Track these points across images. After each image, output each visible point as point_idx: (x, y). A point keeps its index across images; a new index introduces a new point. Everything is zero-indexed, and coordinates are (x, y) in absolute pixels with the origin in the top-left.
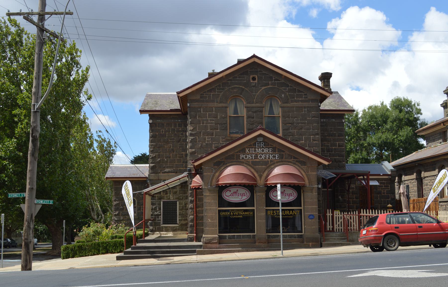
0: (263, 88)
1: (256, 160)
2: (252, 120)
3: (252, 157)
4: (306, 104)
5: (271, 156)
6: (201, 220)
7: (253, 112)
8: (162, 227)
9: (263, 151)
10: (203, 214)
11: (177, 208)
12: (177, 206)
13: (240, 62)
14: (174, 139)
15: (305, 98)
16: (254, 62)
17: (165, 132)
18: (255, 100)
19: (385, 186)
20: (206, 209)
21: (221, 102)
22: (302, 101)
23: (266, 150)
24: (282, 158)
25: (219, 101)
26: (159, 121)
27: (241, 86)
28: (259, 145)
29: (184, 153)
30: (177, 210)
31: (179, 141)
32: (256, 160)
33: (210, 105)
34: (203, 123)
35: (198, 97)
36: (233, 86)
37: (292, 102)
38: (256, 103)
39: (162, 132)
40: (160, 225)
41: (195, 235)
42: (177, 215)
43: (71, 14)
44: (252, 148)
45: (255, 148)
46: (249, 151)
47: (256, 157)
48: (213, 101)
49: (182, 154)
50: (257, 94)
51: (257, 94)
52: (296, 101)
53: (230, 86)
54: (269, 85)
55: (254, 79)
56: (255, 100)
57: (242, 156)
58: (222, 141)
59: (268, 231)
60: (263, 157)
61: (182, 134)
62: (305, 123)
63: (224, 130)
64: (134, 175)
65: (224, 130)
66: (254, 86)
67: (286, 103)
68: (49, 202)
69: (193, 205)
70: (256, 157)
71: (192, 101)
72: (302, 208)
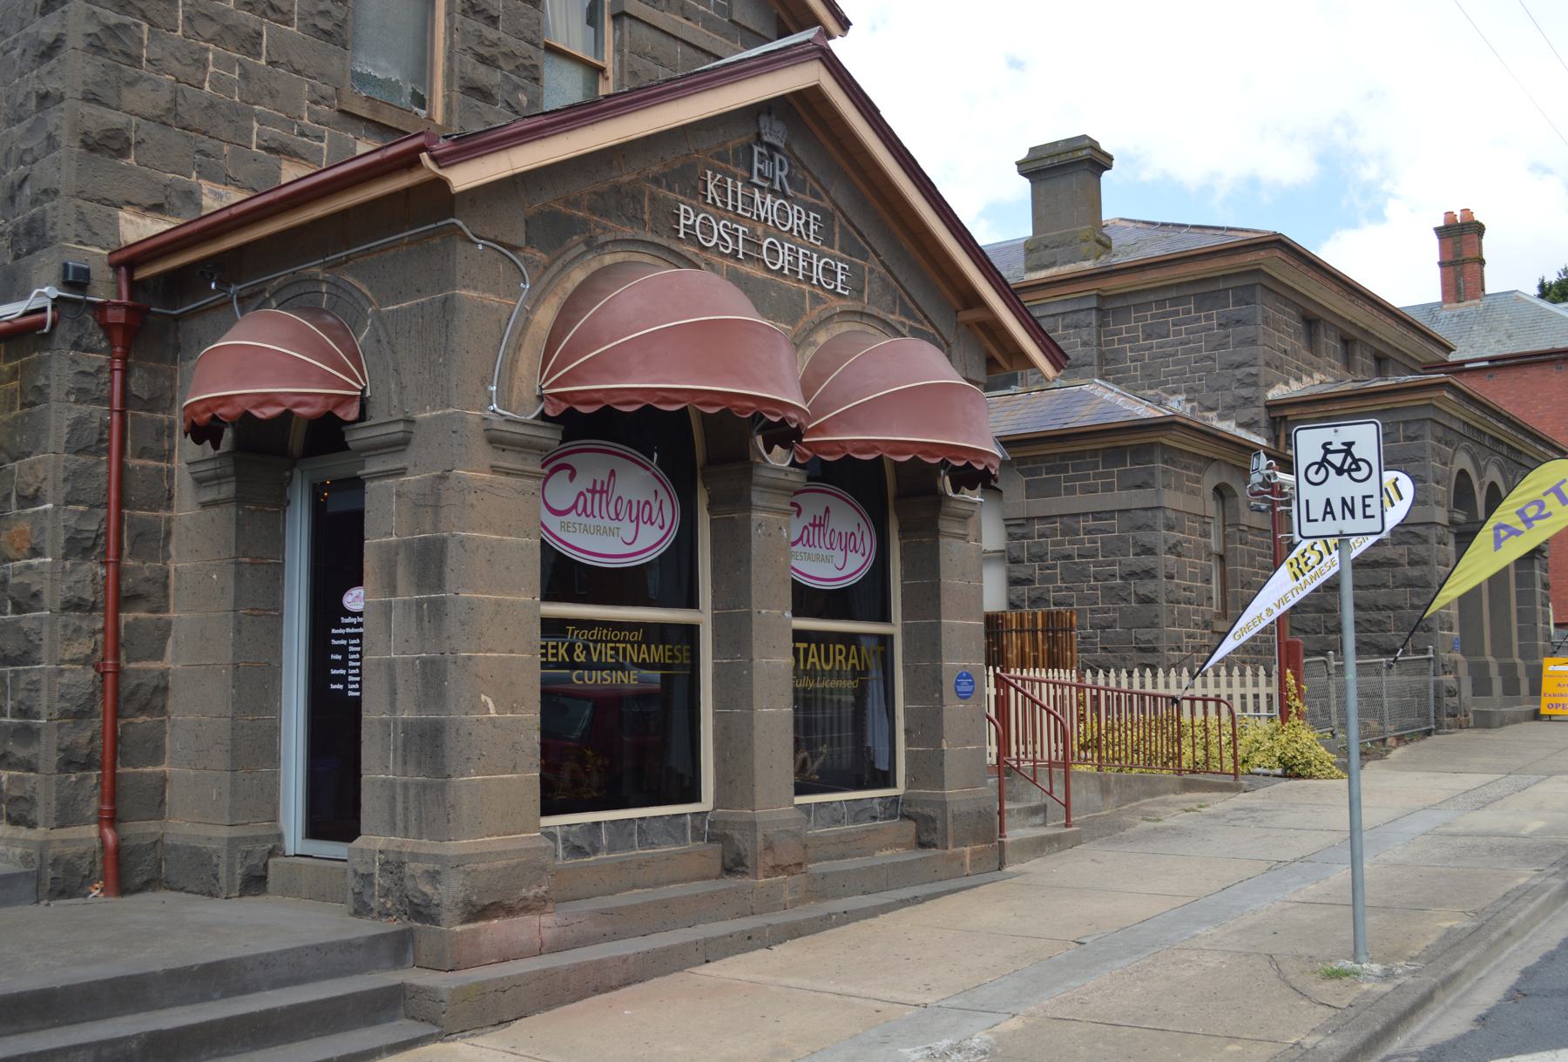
2: (490, 33)
5: (818, 265)
6: (143, 709)
10: (159, 654)
20: (471, 606)
46: (721, 188)
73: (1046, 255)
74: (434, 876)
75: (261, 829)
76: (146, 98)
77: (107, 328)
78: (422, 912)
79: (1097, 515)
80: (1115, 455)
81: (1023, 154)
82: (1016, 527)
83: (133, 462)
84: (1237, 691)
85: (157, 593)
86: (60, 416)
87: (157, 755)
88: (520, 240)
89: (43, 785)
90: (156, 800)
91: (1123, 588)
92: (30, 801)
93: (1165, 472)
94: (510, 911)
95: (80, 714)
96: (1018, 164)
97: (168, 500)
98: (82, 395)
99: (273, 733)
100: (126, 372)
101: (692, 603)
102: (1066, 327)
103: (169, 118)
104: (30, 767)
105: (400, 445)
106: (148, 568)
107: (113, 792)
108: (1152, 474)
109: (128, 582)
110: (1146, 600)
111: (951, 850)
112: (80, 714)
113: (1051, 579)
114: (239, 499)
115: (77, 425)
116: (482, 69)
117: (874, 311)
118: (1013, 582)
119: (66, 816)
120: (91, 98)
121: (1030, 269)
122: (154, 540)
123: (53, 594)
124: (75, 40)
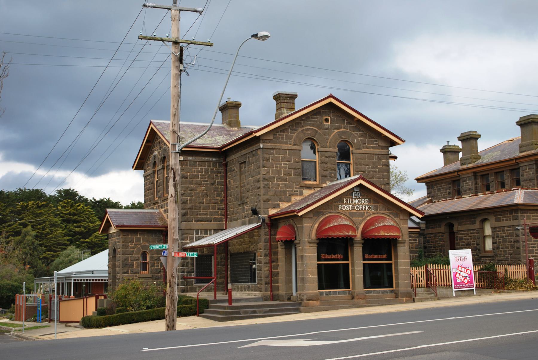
0: (336, 131)
1: (353, 211)
2: (326, 166)
3: (349, 207)
4: (377, 151)
5: (367, 208)
6: (276, 276)
7: (327, 157)
8: (196, 288)
9: (359, 201)
10: (277, 269)
11: (211, 264)
12: (211, 261)
14: (207, 181)
15: (375, 144)
16: (331, 104)
17: (198, 172)
18: (328, 145)
19: (413, 240)
20: (307, 263)
21: (295, 145)
22: (373, 148)
23: (362, 201)
24: (377, 209)
25: (292, 143)
26: (190, 158)
27: (314, 128)
28: (356, 195)
29: (219, 198)
30: (211, 266)
31: (213, 184)
32: (353, 211)
33: (284, 146)
34: (276, 167)
35: (271, 137)
36: (306, 127)
37: (364, 148)
38: (330, 147)
39: (195, 172)
40: (192, 285)
41: (269, 292)
42: (212, 272)
44: (349, 198)
45: (352, 198)
46: (347, 201)
47: (353, 207)
48: (286, 143)
49: (217, 200)
50: (331, 137)
51: (331, 137)
52: (367, 148)
53: (303, 127)
54: (341, 128)
55: (327, 120)
56: (328, 145)
57: (340, 206)
58: (296, 188)
60: (360, 208)
61: (217, 176)
62: (375, 172)
63: (297, 175)
65: (297, 175)
66: (326, 129)
67: (359, 148)
68: (193, 255)
69: (488, 252)
70: (353, 207)
71: (264, 142)
72: (392, 262)
73: (524, 149)
74: (303, 296)
75: (290, 292)
76: (271, 193)
77: (268, 226)
78: (302, 300)
79: (509, 227)
80: (511, 212)
81: (518, 120)
82: (494, 229)
83: (272, 243)
84: (420, 271)
85: (277, 260)
86: (263, 238)
87: (277, 282)
88: (312, 216)
89: (263, 286)
90: (278, 289)
91: (514, 245)
92: (261, 288)
93: (521, 216)
94: (313, 300)
95: (267, 277)
96: (517, 122)
97: (277, 248)
98: (265, 235)
99: (291, 279)
100: (271, 231)
101: (348, 260)
102: (529, 169)
103: (275, 194)
104: (261, 284)
105: (299, 243)
106: (275, 257)
107: (271, 287)
108: (518, 217)
109: (272, 260)
110: (518, 248)
111: (400, 298)
112: (267, 277)
113: (500, 242)
114: (285, 248)
115: (265, 239)
116: (325, 172)
117: (381, 212)
118: (493, 243)
119: (266, 290)
120: (264, 195)
121: (521, 152)
122: (276, 253)
123: (263, 262)
124: (262, 187)
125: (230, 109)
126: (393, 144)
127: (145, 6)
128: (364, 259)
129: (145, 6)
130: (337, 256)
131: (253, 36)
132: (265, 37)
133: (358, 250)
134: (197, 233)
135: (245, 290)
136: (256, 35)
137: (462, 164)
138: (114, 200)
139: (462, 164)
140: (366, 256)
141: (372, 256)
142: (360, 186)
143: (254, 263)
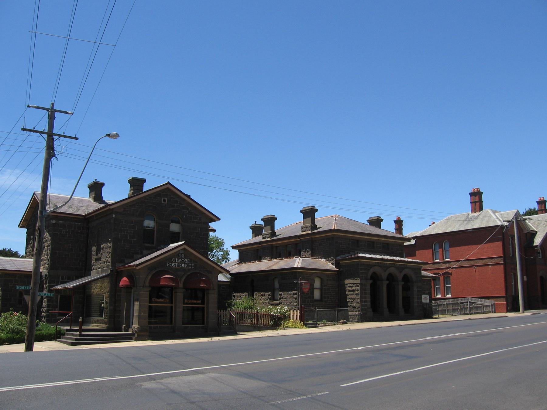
5: (188, 266)
9: (183, 261)
13: (189, 196)
16: (168, 188)
23: (185, 261)
43: (77, 139)
55: (164, 201)
59: (183, 324)
60: (183, 265)
64: (24, 268)
72: (205, 306)
73: (304, 229)
125: (96, 189)
126: (212, 221)
127: (29, 106)
128: (184, 303)
129: (29, 106)
130: (198, 302)
131: (107, 135)
132: (117, 136)
133: (180, 295)
134: (62, 279)
135: (95, 323)
136: (109, 135)
137: (263, 238)
138: (14, 250)
139: (263, 238)
140: (186, 301)
141: (190, 301)
142: (184, 249)
143: (103, 303)
